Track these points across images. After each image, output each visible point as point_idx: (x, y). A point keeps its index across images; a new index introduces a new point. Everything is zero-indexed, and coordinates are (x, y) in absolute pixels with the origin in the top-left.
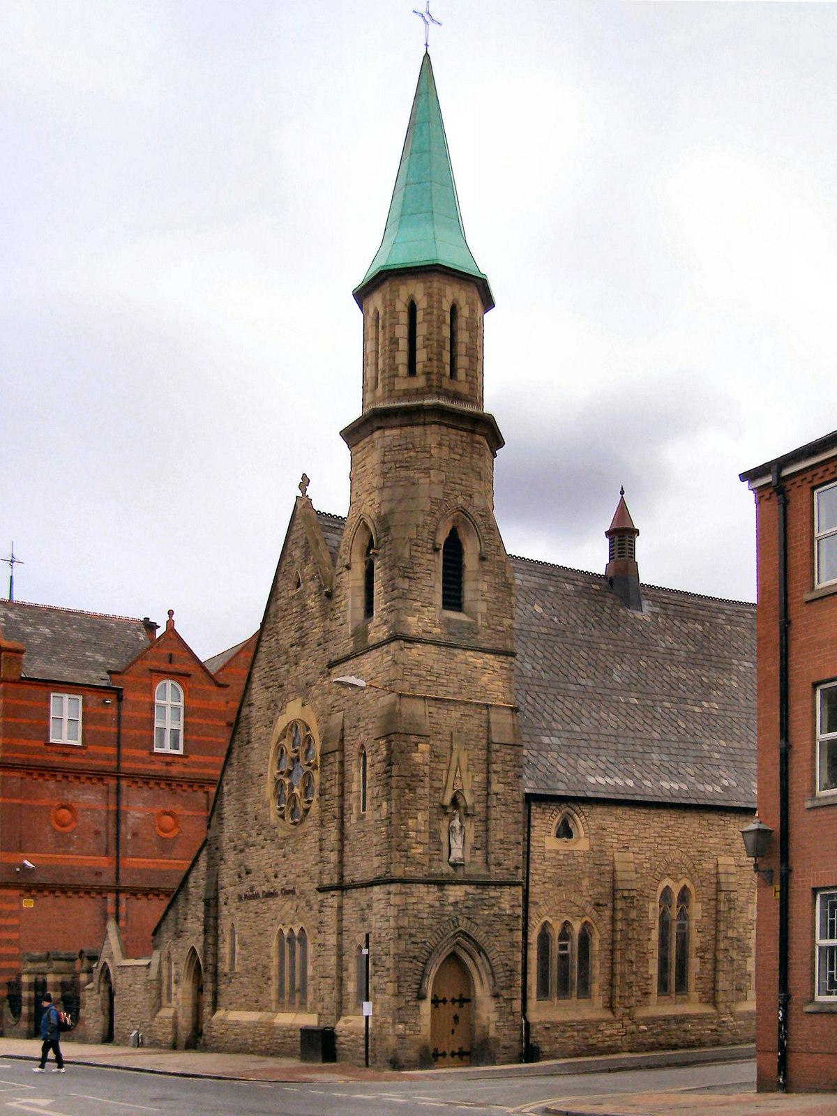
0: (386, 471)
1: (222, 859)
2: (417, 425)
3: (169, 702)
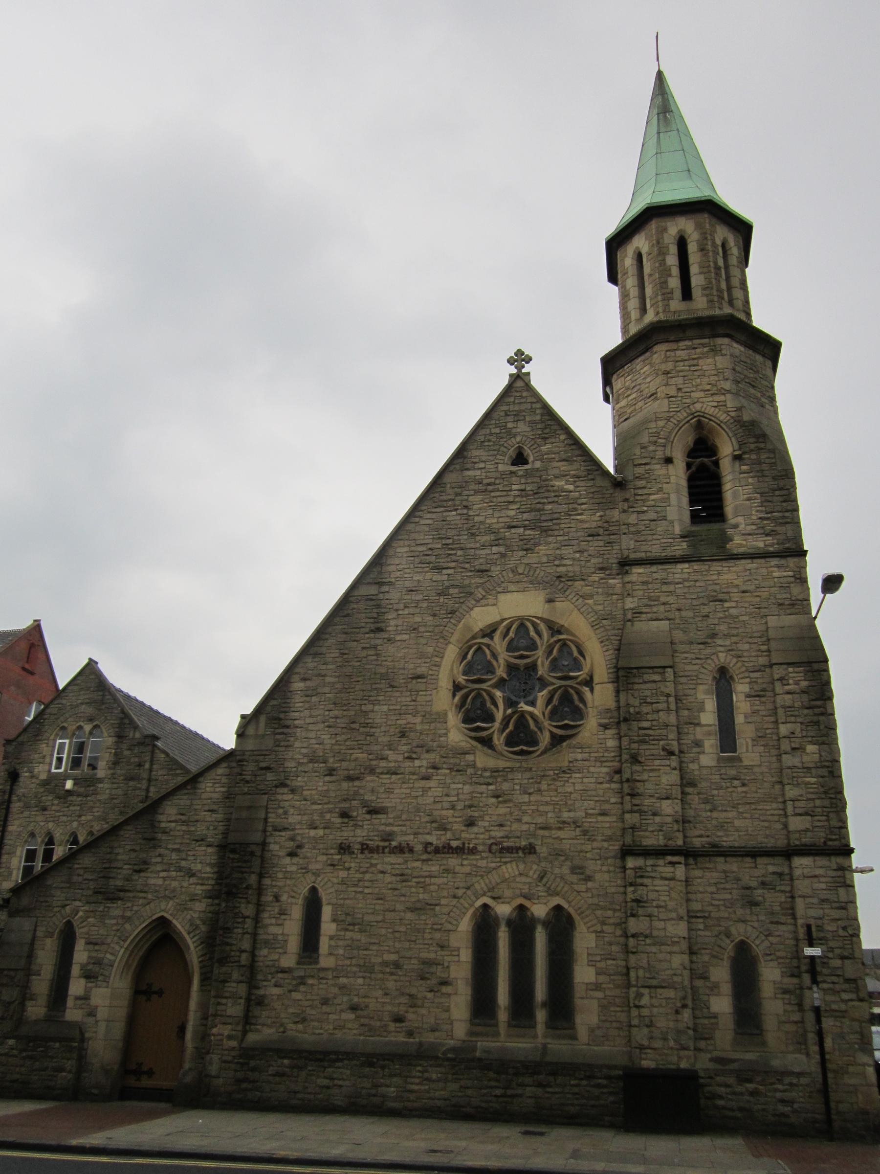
1: (283, 785)
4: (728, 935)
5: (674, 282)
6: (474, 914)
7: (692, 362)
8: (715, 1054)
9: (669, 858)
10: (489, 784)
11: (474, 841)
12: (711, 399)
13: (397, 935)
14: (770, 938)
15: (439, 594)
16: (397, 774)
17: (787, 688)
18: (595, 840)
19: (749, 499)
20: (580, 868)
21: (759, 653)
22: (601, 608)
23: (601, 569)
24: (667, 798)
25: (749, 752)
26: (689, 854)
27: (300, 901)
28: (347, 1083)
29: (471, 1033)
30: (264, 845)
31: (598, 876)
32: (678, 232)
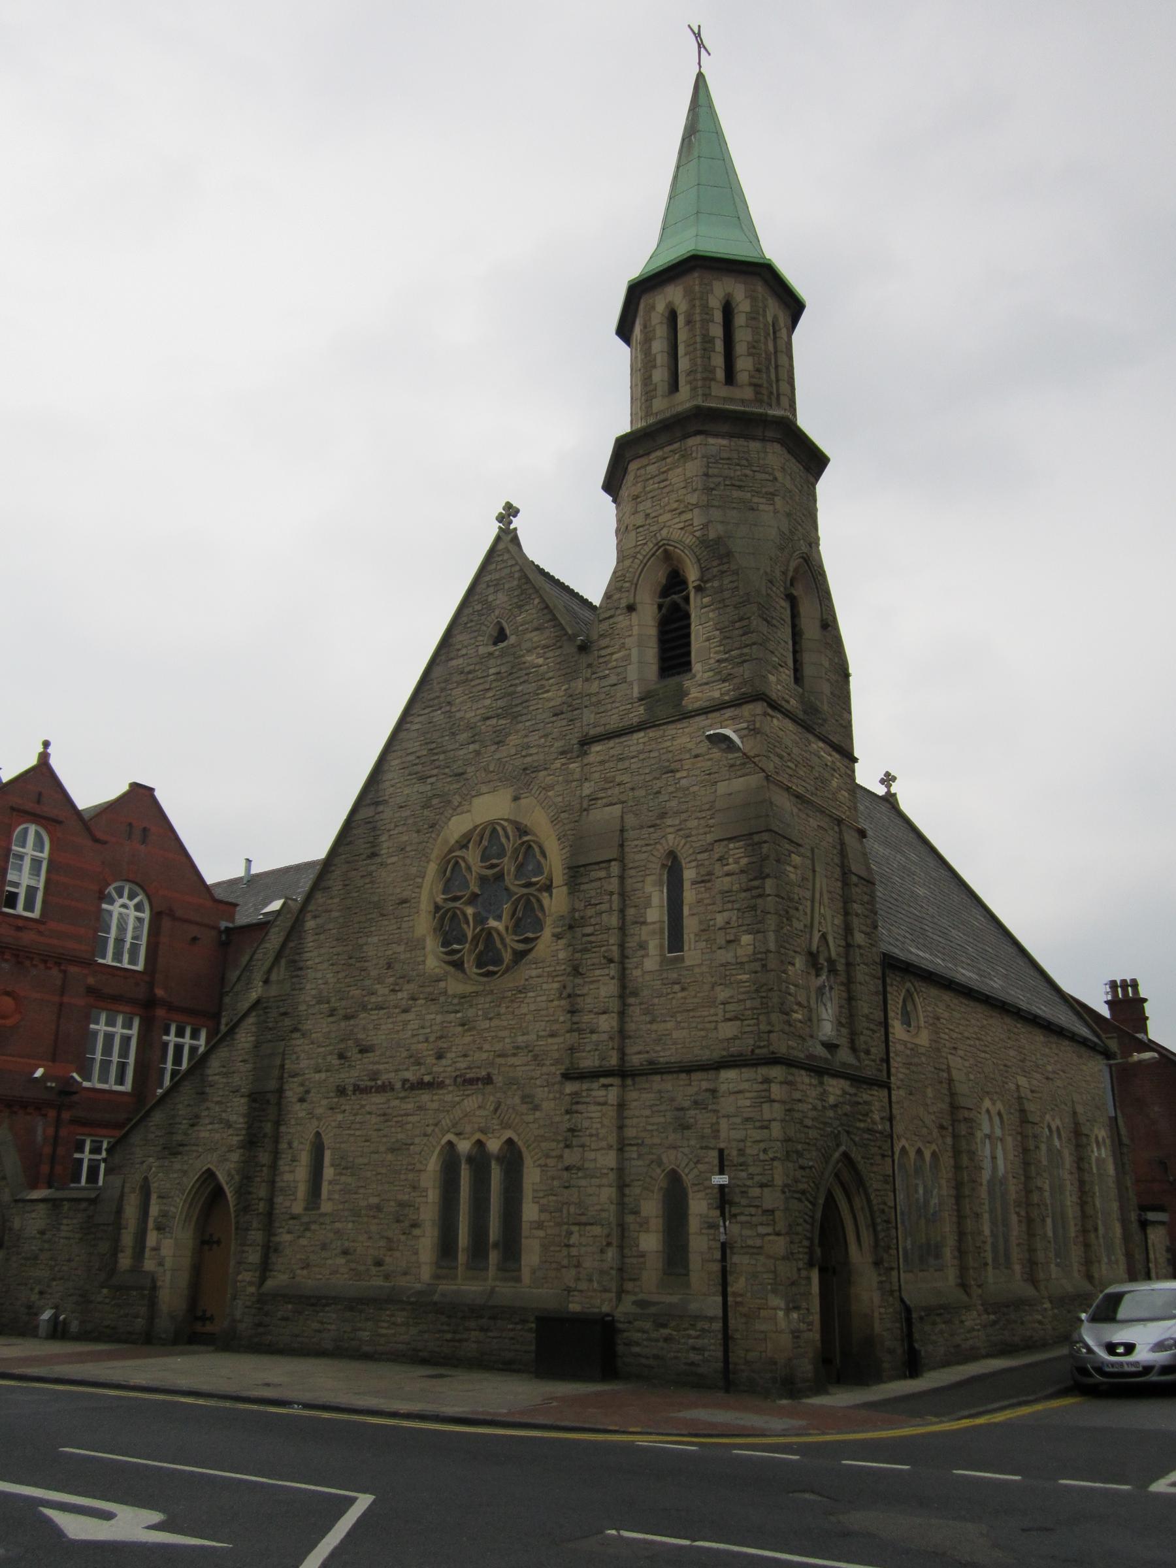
0: (712, 486)
1: (296, 1030)
2: (754, 438)
3: (29, 850)
4: (660, 1163)
5: (718, 361)
6: (439, 1154)
7: (662, 477)
8: (640, 1296)
9: (603, 1081)
10: (457, 1012)
11: (443, 1075)
12: (677, 520)
13: (379, 1177)
14: (699, 1166)
15: (423, 807)
16: (383, 1008)
17: (726, 868)
18: (543, 1065)
19: (708, 639)
20: (528, 1096)
21: (707, 829)
22: (560, 799)
23: (563, 753)
24: (604, 1013)
25: (693, 953)
26: (624, 1073)
27: (308, 1147)
28: (333, 1327)
29: (437, 1277)
30: (280, 1091)
31: (545, 1105)
32: (667, 306)
